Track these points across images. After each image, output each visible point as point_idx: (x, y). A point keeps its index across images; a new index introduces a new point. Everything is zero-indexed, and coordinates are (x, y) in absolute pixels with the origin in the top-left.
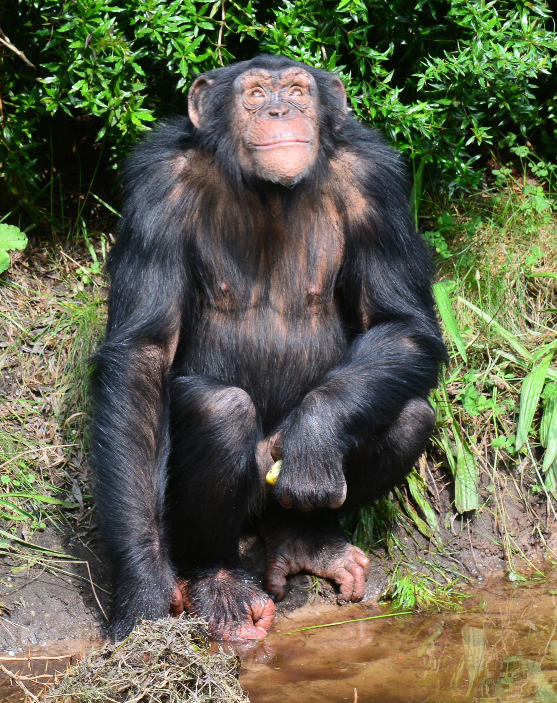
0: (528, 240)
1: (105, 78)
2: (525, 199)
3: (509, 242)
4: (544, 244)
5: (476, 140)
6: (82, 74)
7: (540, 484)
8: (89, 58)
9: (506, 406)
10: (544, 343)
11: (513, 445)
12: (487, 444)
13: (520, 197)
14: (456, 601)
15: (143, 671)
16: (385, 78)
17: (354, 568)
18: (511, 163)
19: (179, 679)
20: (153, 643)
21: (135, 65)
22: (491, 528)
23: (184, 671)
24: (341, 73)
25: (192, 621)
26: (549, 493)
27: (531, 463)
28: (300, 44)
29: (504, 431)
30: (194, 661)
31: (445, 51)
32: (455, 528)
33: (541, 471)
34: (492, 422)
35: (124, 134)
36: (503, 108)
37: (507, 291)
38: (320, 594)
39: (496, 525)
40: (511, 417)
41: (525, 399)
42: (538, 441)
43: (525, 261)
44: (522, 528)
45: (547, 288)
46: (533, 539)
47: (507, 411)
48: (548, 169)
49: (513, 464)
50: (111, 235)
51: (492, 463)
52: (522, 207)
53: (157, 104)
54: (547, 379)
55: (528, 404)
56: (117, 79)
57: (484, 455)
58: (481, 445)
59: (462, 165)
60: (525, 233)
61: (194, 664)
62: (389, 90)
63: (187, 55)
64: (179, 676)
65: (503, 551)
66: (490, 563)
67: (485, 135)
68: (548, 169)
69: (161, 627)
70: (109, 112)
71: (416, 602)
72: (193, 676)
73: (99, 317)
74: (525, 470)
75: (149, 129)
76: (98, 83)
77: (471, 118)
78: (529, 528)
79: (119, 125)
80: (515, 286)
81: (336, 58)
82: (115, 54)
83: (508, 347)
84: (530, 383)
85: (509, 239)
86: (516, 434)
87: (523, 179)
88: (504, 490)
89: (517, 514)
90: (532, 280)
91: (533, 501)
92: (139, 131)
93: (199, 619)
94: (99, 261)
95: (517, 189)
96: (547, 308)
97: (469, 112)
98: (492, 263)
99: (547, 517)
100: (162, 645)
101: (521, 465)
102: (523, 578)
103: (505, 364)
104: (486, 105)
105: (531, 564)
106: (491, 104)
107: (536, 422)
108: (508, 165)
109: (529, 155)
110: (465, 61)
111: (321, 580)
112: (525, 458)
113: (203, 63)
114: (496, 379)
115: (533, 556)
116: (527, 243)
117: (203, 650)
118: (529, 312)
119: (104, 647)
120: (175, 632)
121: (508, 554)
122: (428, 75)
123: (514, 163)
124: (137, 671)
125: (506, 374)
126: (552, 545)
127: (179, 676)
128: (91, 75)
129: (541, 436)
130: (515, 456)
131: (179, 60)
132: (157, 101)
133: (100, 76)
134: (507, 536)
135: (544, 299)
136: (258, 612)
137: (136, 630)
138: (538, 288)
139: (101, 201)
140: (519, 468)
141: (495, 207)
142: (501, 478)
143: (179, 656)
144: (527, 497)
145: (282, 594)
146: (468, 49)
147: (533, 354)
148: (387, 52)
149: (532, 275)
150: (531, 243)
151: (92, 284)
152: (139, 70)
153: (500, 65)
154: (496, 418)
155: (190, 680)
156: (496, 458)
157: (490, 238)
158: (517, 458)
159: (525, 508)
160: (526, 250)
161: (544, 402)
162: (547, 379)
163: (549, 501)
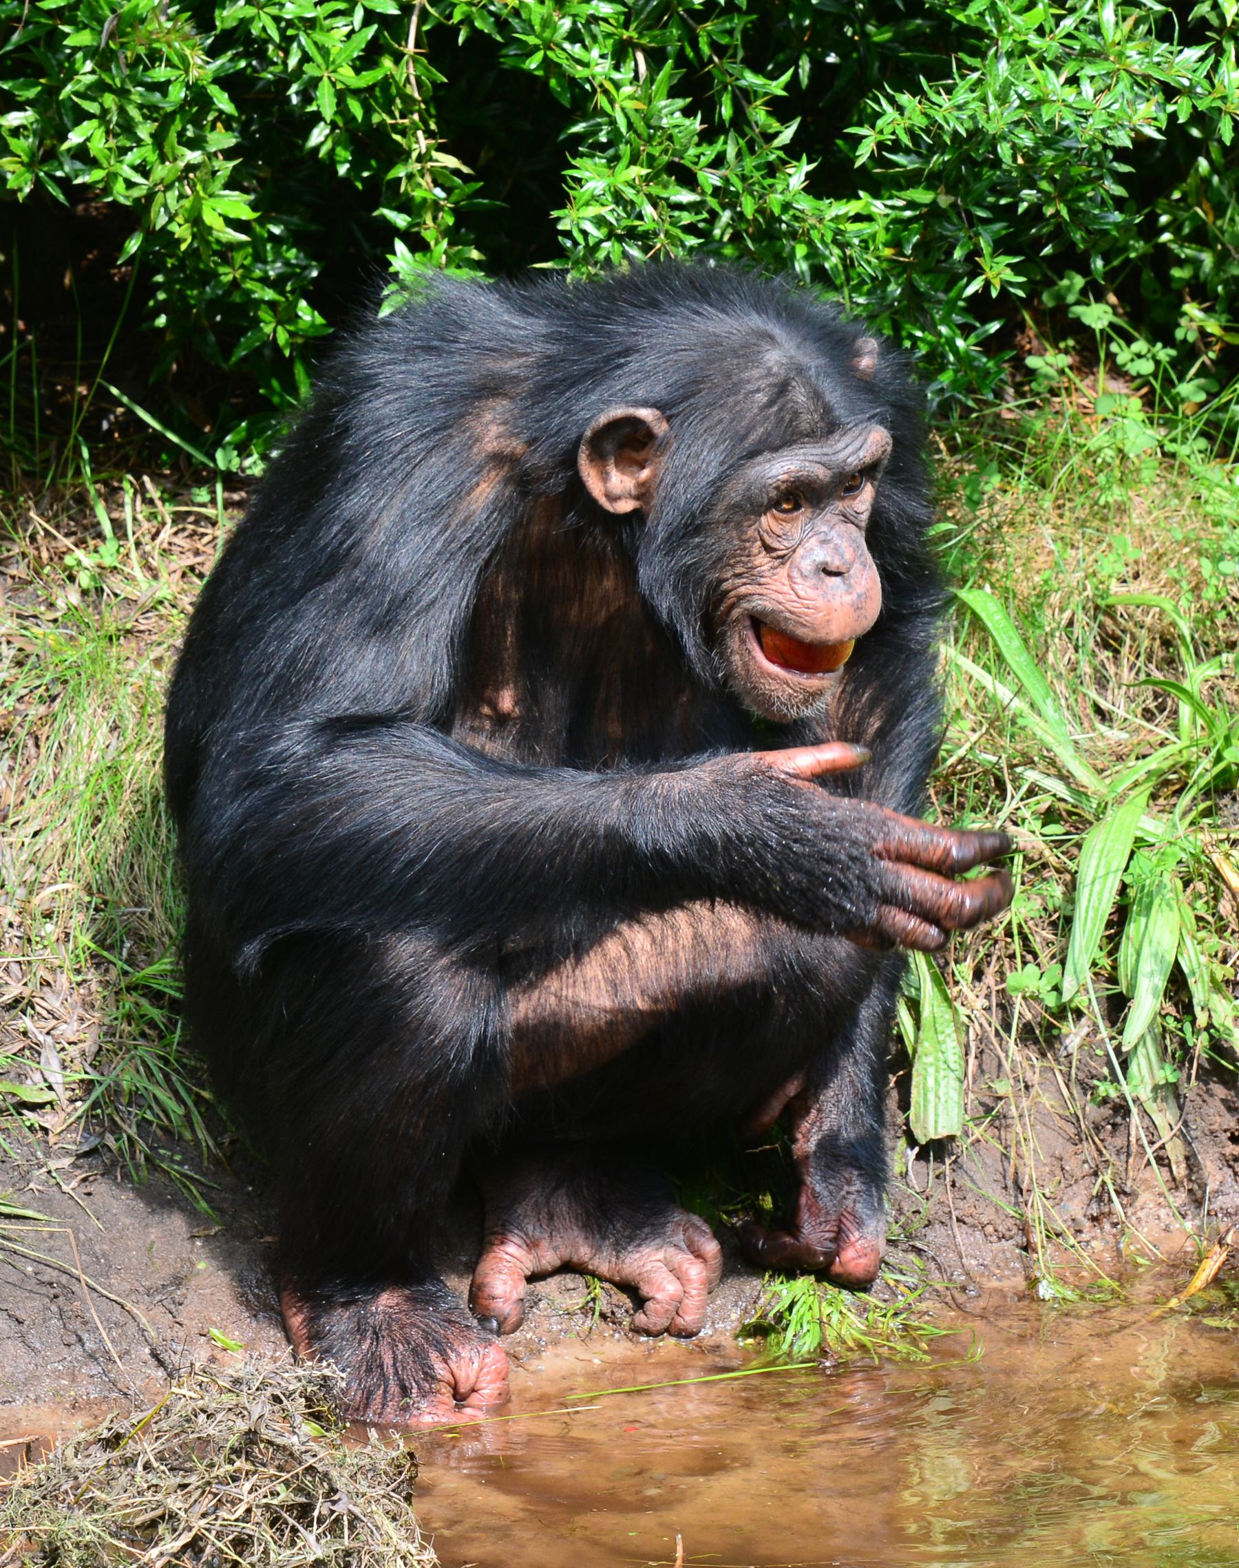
0: (1104, 519)
1: (144, 116)
2: (1100, 426)
3: (1059, 522)
4: (1141, 530)
5: (987, 285)
6: (92, 107)
7: (1115, 1080)
8: (108, 70)
9: (1044, 898)
10: (1133, 756)
11: (1057, 989)
12: (997, 983)
13: (1088, 419)
14: (914, 1342)
15: (193, 1480)
16: (776, 134)
17: (686, 1266)
18: (1071, 343)
19: (275, 1502)
20: (219, 1417)
21: (214, 90)
22: (999, 1177)
23: (287, 1483)
24: (678, 114)
25: (311, 1369)
26: (1136, 1100)
27: (1095, 1030)
28: (588, 41)
29: (1036, 956)
30: (311, 1461)
31: (922, 79)
32: (917, 1174)
33: (1118, 1050)
34: (1009, 933)
35: (183, 247)
36: (1052, 216)
37: (1053, 636)
38: (603, 1316)
39: (1011, 1170)
40: (1054, 924)
41: (1089, 880)
42: (1113, 980)
43: (1096, 567)
44: (1069, 1181)
45: (1144, 631)
46: (1094, 1206)
47: (1045, 909)
48: (1154, 358)
49: (1055, 1032)
50: (146, 479)
51: (1007, 1027)
52: (1092, 445)
53: (261, 182)
54: (1138, 840)
55: (1095, 896)
56: (173, 121)
57: (988, 1009)
58: (981, 987)
59: (960, 343)
60: (1096, 503)
61: (311, 1467)
62: (785, 163)
63: (334, 71)
64: (274, 1494)
65: (1025, 1229)
66: (994, 1258)
67: (1009, 275)
68: (1154, 358)
69: (237, 1382)
70: (150, 196)
71: (823, 1339)
72: (308, 1495)
73: (113, 665)
74: (1081, 1047)
75: (243, 238)
76: (127, 127)
77: (977, 234)
78: (1088, 1180)
79: (173, 227)
80: (1071, 624)
81: (671, 76)
82: (170, 64)
83: (1053, 763)
84: (1099, 847)
85: (1061, 516)
86: (1063, 962)
87: (1096, 381)
88: (1033, 1092)
89: (1061, 1147)
90: (1110, 611)
91: (1098, 1119)
92: (218, 242)
93: (324, 1364)
94: (119, 539)
95: (1083, 401)
96: (1142, 677)
97: (972, 221)
98: (1019, 570)
99: (1129, 1155)
100: (239, 1421)
101: (1073, 1035)
102: (1069, 1295)
103: (1045, 802)
104: (1014, 206)
105: (1089, 1261)
106: (1025, 205)
107: (1110, 938)
108: (1062, 345)
109: (1111, 325)
110: (966, 103)
111: (607, 1285)
112: (1083, 1020)
113: (370, 89)
114: (1023, 835)
115: (1094, 1243)
116: (1103, 526)
117: (332, 1435)
118: (1102, 682)
119: (106, 1424)
120: (268, 1394)
121: (1038, 1238)
122: (881, 132)
123: (1077, 342)
124: (179, 1480)
125: (1044, 825)
126: (1139, 1219)
127: (274, 1494)
128: (114, 108)
129: (1121, 970)
130: (1061, 1012)
131: (315, 82)
132: (262, 175)
133: (134, 112)
134: (1036, 1197)
135: (1138, 657)
136: (468, 1377)
137: (180, 1386)
138: (1123, 631)
139: (125, 399)
140: (1067, 1041)
141: (1030, 441)
142: (1025, 1064)
143: (279, 1448)
144: (1084, 1109)
145: (513, 1319)
146: (975, 76)
147: (1108, 781)
148: (786, 77)
149: (1110, 601)
150: (1111, 526)
151: (99, 591)
152: (223, 101)
153: (1047, 113)
154: (1020, 926)
155: (301, 1505)
156: (1016, 1016)
157: (1017, 512)
158: (1064, 1018)
159: (1078, 1134)
160: (1099, 542)
161: (1131, 893)
162: (1138, 840)
163: (1135, 1119)
